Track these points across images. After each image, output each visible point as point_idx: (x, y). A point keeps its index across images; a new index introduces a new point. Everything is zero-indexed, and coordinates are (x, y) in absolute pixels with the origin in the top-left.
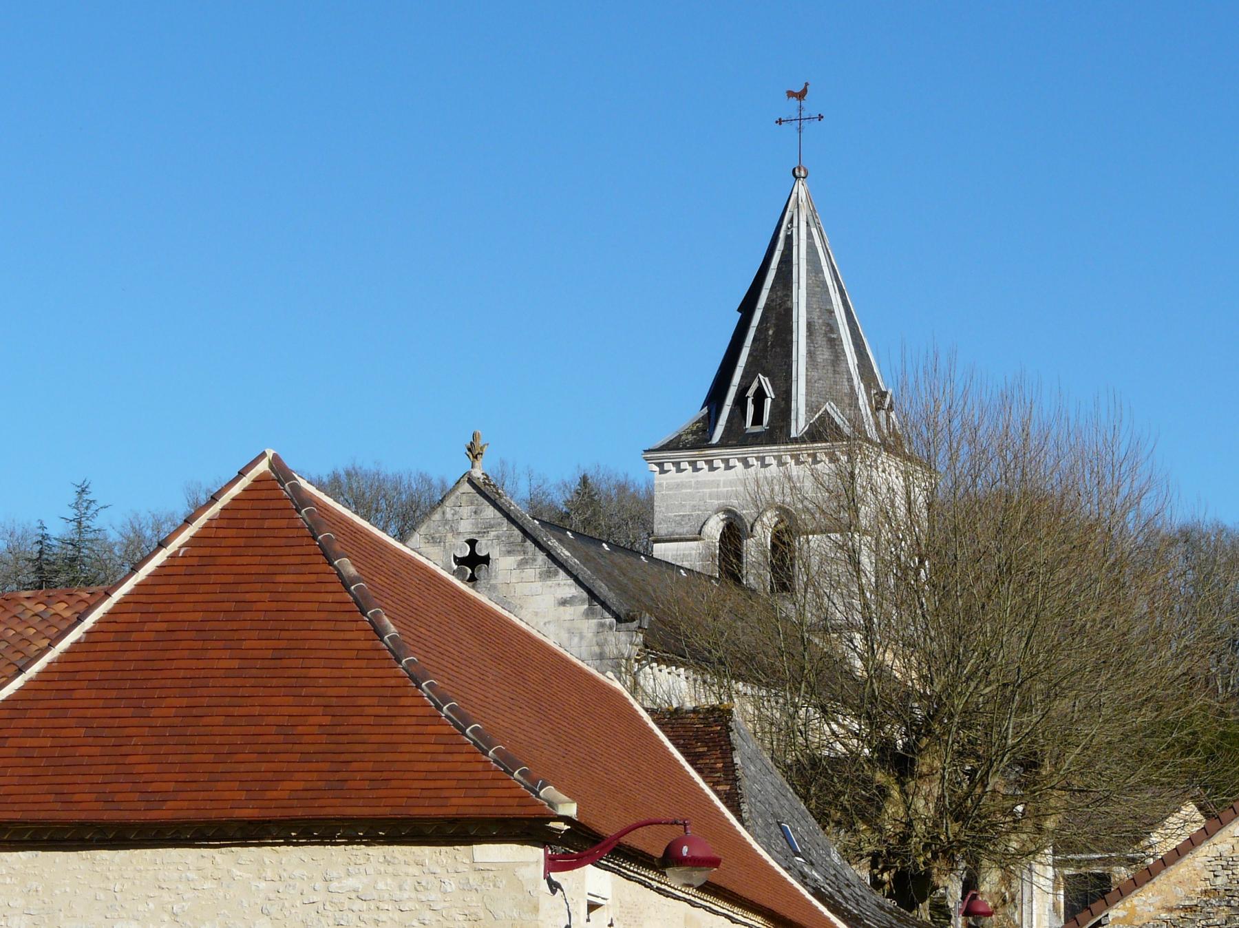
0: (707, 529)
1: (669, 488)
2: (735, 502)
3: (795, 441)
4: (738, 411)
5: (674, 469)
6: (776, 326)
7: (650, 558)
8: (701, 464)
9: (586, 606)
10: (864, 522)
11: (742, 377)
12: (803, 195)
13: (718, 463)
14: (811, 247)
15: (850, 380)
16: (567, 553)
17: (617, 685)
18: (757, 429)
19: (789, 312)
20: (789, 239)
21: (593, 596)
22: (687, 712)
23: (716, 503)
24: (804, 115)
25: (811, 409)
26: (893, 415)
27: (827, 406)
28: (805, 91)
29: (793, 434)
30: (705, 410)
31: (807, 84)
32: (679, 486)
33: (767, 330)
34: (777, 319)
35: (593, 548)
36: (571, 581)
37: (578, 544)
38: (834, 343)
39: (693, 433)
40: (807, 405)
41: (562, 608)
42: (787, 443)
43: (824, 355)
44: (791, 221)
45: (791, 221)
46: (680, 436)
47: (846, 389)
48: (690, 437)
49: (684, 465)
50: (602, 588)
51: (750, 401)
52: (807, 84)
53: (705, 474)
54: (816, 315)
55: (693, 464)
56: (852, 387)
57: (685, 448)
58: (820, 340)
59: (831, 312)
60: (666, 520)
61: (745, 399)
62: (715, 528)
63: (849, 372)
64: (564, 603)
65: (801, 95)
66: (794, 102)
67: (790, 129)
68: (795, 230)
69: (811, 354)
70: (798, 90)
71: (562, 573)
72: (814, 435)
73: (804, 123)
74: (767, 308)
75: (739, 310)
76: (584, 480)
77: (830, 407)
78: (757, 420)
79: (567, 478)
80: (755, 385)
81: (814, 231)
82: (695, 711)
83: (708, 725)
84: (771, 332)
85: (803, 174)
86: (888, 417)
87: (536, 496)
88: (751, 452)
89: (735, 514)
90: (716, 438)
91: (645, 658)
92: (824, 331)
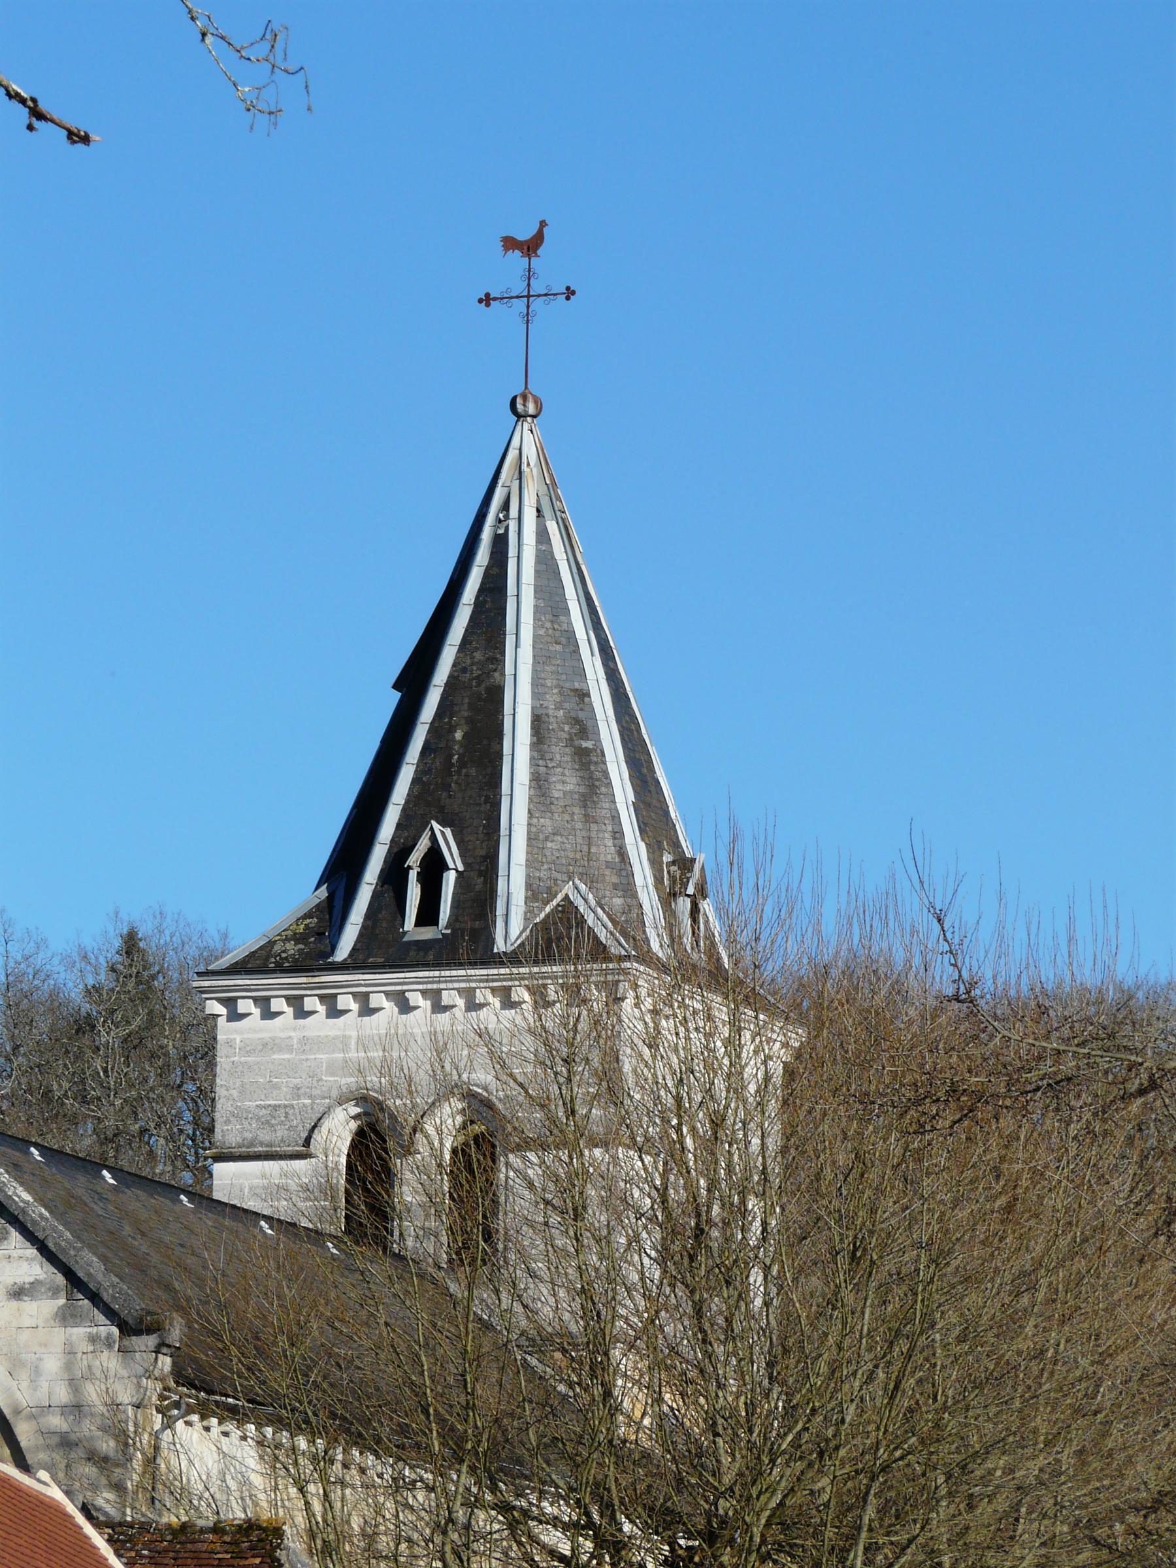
0: (319, 1137)
1: (247, 1049)
2: (373, 1079)
3: (513, 959)
4: (389, 897)
5: (256, 1012)
6: (470, 721)
7: (205, 1200)
8: (311, 1003)
9: (62, 1301)
11: (399, 826)
12: (530, 452)
13: (346, 1001)
14: (545, 561)
15: (618, 834)
16: (27, 1197)
17: (56, 1493)
18: (427, 933)
19: (496, 694)
20: (500, 543)
21: (75, 1282)
22: (202, 1531)
23: (349, 1081)
24: (538, 287)
25: (534, 893)
26: (706, 906)
27: (568, 889)
29: (500, 946)
30: (323, 892)
31: (543, 224)
32: (268, 1046)
33: (452, 729)
34: (471, 707)
35: (82, 1179)
36: (32, 1252)
37: (50, 1172)
38: (588, 760)
39: (298, 938)
40: (529, 886)
41: (14, 1304)
42: (484, 964)
43: (566, 783)
44: (506, 506)
45: (506, 506)
46: (271, 943)
47: (608, 851)
48: (291, 948)
49: (278, 1004)
50: (90, 1265)
51: (413, 875)
52: (543, 224)
53: (319, 1024)
54: (551, 700)
55: (296, 1002)
56: (622, 853)
57: (280, 970)
58: (559, 752)
59: (583, 695)
60: (239, 1115)
61: (404, 876)
62: (339, 1132)
63: (616, 818)
64: (18, 1293)
65: (531, 247)
67: (508, 315)
68: (513, 526)
69: (539, 782)
70: (524, 233)
71: (15, 1236)
72: (558, 936)
73: (536, 304)
74: (452, 685)
75: (396, 686)
76: (131, 944)
77: (575, 891)
78: (428, 915)
79: (89, 943)
80: (423, 845)
81: (552, 527)
82: (217, 1529)
83: (240, 1555)
84: (458, 735)
85: (531, 409)
86: (695, 911)
87: (19, 979)
88: (413, 982)
89: (381, 1106)
90: (343, 951)
91: (177, 1405)
92: (567, 734)
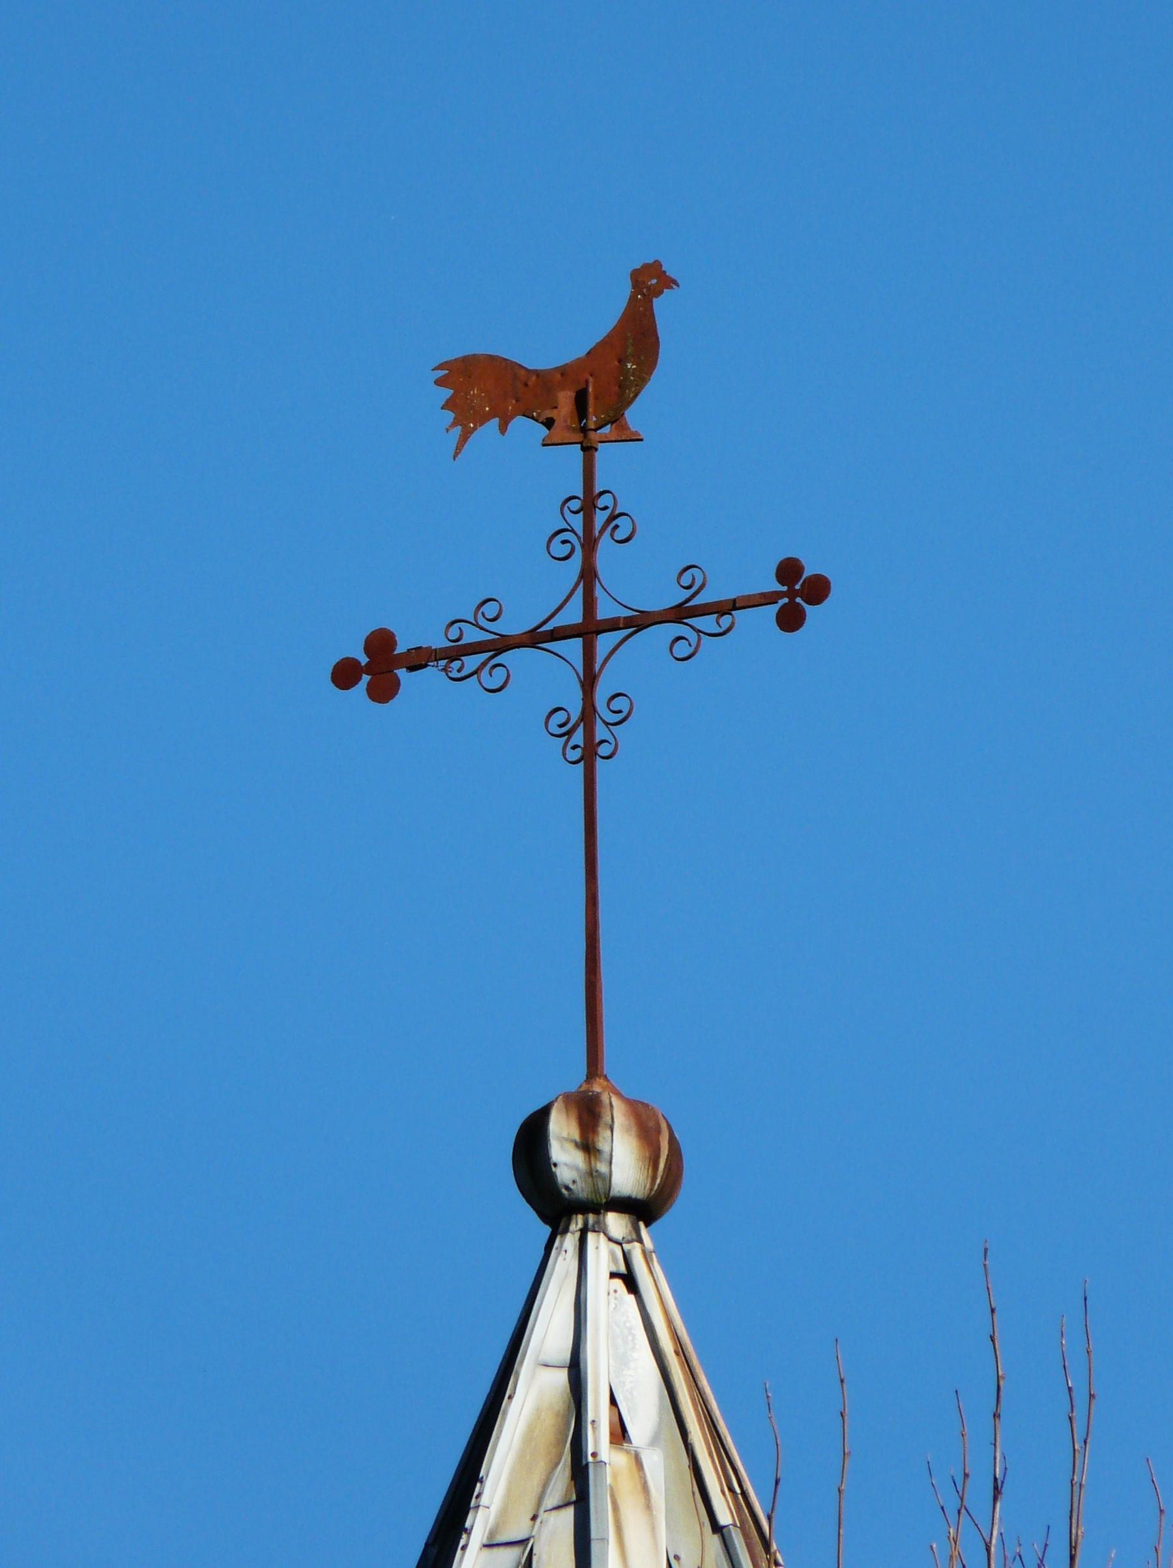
10: (654, 1255)
12: (626, 1371)
28: (633, 345)
31: (649, 282)
52: (649, 282)
65: (594, 395)
66: (528, 464)
70: (558, 334)
85: (626, 1171)
